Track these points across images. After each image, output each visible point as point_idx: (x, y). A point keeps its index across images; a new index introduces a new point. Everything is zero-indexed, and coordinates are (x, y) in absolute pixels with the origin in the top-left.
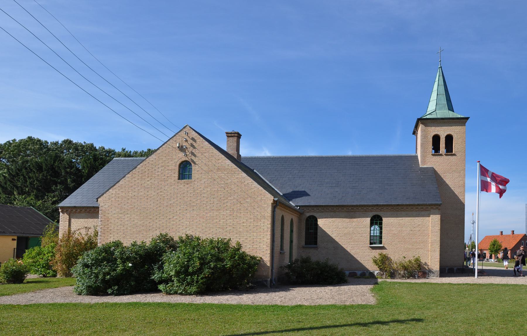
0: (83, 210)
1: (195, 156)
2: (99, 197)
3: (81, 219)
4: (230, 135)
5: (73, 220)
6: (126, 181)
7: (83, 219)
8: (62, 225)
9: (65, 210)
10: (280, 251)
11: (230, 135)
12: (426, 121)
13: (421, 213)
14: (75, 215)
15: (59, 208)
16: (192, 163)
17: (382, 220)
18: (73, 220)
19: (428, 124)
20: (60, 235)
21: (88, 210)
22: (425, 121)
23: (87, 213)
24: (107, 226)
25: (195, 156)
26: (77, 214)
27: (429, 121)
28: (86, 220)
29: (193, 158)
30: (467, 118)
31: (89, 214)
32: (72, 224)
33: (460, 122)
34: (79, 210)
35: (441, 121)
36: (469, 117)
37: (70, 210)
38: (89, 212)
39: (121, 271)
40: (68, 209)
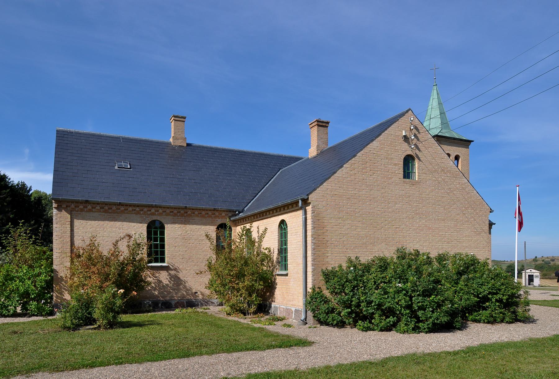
0: (98, 208)
1: (419, 150)
2: (311, 193)
3: (91, 220)
4: (321, 124)
5: (77, 222)
6: (344, 173)
7: (95, 221)
8: (57, 229)
9: (64, 206)
10: (521, 267)
11: (321, 124)
12: (441, 138)
13: (188, 219)
14: (80, 214)
15: (53, 201)
16: (416, 157)
17: (164, 228)
18: (77, 222)
19: (442, 142)
20: (56, 247)
21: (106, 208)
22: (440, 138)
23: (103, 212)
24: (322, 236)
25: (419, 150)
26: (83, 212)
27: (443, 139)
28: (101, 223)
29: (417, 151)
30: (470, 141)
31: (106, 214)
32: (75, 228)
33: (466, 144)
34: (89, 207)
35: (452, 140)
36: (474, 141)
37: (73, 206)
38: (106, 212)
39: (476, 302)
40: (70, 204)
